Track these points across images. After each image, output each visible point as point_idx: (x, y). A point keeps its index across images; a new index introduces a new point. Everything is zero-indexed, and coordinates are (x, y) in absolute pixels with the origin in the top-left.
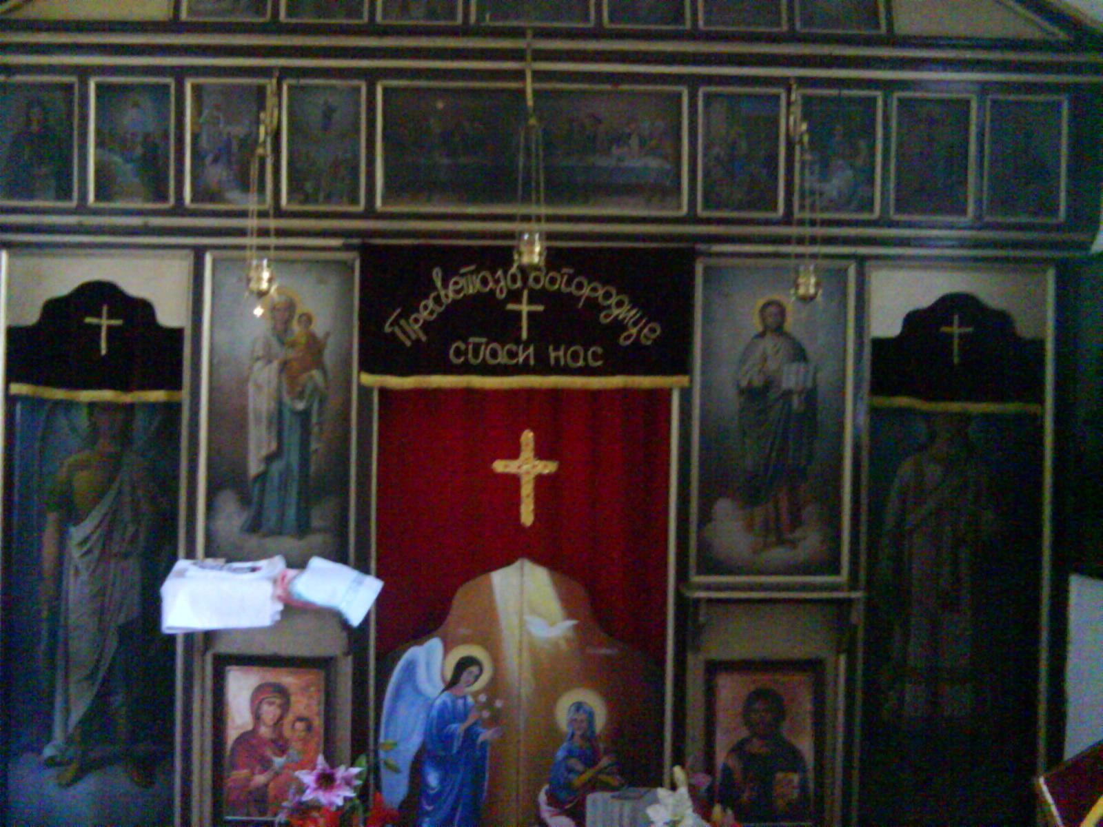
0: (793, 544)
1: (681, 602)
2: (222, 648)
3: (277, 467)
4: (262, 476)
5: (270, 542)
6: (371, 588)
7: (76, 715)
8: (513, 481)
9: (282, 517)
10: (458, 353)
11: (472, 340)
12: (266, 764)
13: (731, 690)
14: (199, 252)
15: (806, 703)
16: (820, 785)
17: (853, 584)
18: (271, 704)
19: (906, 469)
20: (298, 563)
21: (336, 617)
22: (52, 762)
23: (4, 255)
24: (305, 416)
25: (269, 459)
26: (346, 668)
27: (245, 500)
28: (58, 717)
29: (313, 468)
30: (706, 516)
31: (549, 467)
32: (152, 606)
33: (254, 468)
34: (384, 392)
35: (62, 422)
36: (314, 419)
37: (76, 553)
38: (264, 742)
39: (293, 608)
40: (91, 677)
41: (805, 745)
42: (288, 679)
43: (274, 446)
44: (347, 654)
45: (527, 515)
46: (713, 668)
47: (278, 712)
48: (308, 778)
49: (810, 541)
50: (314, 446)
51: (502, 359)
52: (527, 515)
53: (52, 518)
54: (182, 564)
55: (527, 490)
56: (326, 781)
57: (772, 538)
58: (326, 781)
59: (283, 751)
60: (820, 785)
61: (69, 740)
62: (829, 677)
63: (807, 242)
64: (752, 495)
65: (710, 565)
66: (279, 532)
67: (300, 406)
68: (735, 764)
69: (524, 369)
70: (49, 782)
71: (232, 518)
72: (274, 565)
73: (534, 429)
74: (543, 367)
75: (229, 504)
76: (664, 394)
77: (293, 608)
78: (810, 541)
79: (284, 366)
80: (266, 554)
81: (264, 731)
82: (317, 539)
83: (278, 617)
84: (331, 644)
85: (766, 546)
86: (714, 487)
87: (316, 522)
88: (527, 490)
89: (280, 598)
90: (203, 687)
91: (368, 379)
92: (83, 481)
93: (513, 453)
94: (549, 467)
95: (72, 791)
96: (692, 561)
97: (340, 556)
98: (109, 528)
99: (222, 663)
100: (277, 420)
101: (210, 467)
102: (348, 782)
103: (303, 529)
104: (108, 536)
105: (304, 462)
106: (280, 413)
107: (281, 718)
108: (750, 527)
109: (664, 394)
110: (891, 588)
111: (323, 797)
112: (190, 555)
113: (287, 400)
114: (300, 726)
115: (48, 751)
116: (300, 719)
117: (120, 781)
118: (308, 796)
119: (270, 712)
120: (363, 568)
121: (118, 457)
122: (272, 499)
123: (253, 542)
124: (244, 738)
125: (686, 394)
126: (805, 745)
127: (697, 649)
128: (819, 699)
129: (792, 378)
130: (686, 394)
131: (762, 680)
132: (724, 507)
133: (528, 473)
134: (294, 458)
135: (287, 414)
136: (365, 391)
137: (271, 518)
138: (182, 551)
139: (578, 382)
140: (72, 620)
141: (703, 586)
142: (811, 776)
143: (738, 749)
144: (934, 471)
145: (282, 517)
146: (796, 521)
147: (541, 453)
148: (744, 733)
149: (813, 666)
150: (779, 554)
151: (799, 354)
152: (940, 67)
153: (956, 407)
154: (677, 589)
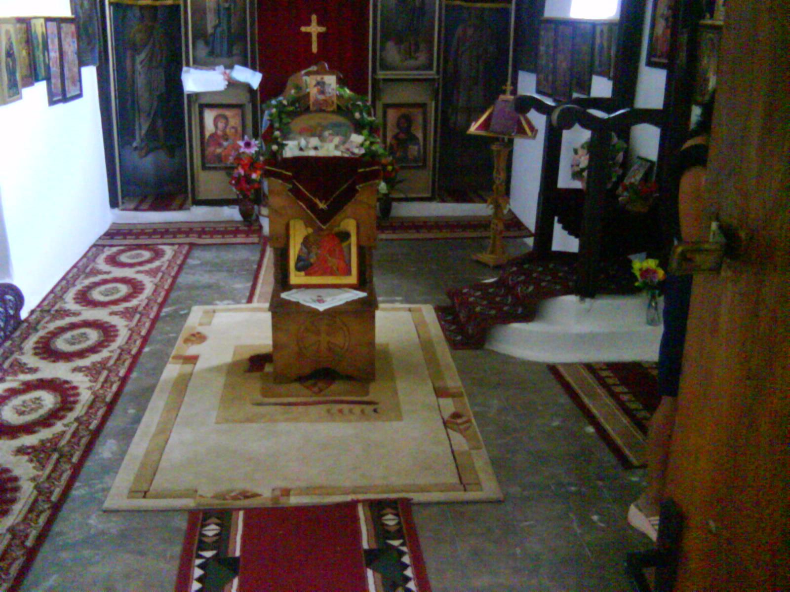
0: (416, 59)
1: (374, 80)
2: (203, 101)
3: (219, 30)
4: (213, 35)
5: (217, 60)
7: (143, 132)
8: (309, 35)
9: (221, 50)
12: (220, 145)
13: (392, 114)
15: (420, 118)
16: (425, 152)
17: (438, 72)
18: (221, 122)
19: (459, 31)
20: (231, 67)
21: (248, 87)
22: (136, 148)
24: (228, 9)
25: (215, 27)
26: (249, 108)
27: (207, 43)
28: (137, 133)
29: (233, 31)
30: (383, 49)
31: (322, 29)
32: (178, 85)
33: (210, 30)
35: (129, 12)
36: (232, 11)
37: (139, 67)
38: (219, 137)
39: (232, 84)
40: (149, 115)
41: (420, 136)
42: (228, 113)
43: (217, 22)
44: (249, 102)
45: (315, 49)
46: (387, 106)
47: (224, 125)
48: (241, 143)
49: (422, 58)
50: (232, 21)
52: (315, 49)
53: (129, 53)
54: (185, 69)
55: (314, 39)
56: (248, 145)
57: (408, 56)
58: (248, 145)
59: (227, 140)
60: (425, 152)
61: (142, 141)
62: (428, 109)
63: (26, 413)
64: (399, 41)
65: (385, 67)
66: (221, 55)
67: (227, 5)
68: (394, 142)
70: (135, 156)
71: (203, 51)
72: (221, 68)
73: (300, 26)
75: (201, 44)
77: (232, 84)
78: (422, 58)
80: (218, 64)
81: (220, 133)
82: (235, 58)
83: (226, 87)
84: (243, 98)
85: (406, 59)
86: (386, 37)
87: (235, 51)
88: (314, 39)
89: (226, 80)
90: (195, 115)
92: (139, 37)
93: (308, 24)
94: (322, 29)
95: (144, 159)
96: (378, 64)
97: (245, 64)
98: (151, 58)
99: (203, 107)
100: (218, 12)
101: (193, 32)
102: (256, 145)
103: (230, 54)
104: (151, 60)
105: (229, 31)
106: (219, 10)
107: (226, 127)
108: (399, 52)
110: (526, 266)
111: (247, 151)
112: (188, 65)
114: (233, 131)
115: (135, 145)
116: (233, 127)
117: (162, 156)
118: (242, 150)
119: (221, 125)
120: (254, 68)
121: (153, 28)
122: (218, 40)
123: (212, 59)
124: (212, 136)
126: (420, 136)
127: (380, 99)
128: (425, 121)
131: (403, 111)
132: (390, 45)
133: (314, 32)
134: (225, 26)
135: (222, 9)
137: (218, 51)
138: (184, 62)
140: (140, 93)
141: (381, 75)
142: (422, 148)
143: (395, 137)
144: (470, 32)
145: (221, 50)
146: (417, 49)
147: (320, 23)
148: (397, 131)
149: (423, 106)
150: (412, 63)
153: (479, 5)
154: (372, 76)
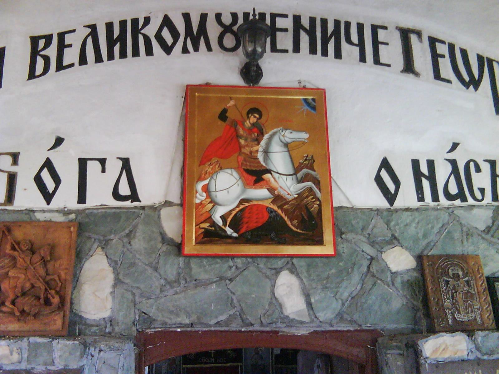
6: (480, 371)
10: (200, 360)
11: (203, 358)
14: (483, 323)
23: (3, 342)
34: (187, 368)
51: (208, 361)
69: (213, 363)
74: (215, 362)
76: (237, 367)
79: (168, 364)
91: (184, 366)
109: (237, 367)
113: (169, 370)
125: (241, 366)
129: (260, 362)
130: (241, 366)
136: (183, 368)
139: (207, 366)
151: (262, 358)
152: (415, 72)
